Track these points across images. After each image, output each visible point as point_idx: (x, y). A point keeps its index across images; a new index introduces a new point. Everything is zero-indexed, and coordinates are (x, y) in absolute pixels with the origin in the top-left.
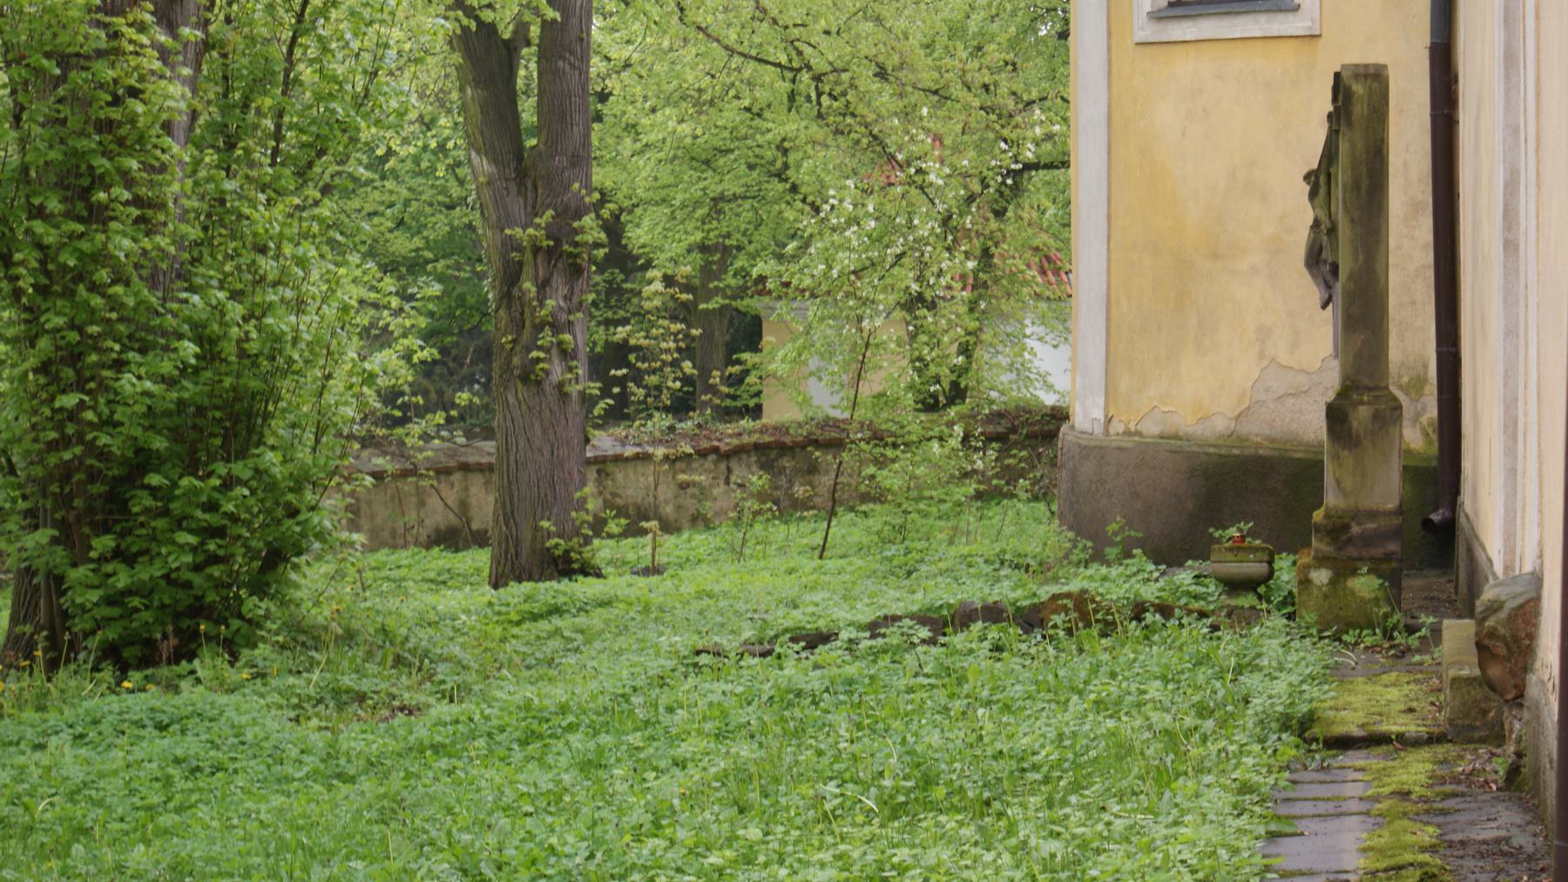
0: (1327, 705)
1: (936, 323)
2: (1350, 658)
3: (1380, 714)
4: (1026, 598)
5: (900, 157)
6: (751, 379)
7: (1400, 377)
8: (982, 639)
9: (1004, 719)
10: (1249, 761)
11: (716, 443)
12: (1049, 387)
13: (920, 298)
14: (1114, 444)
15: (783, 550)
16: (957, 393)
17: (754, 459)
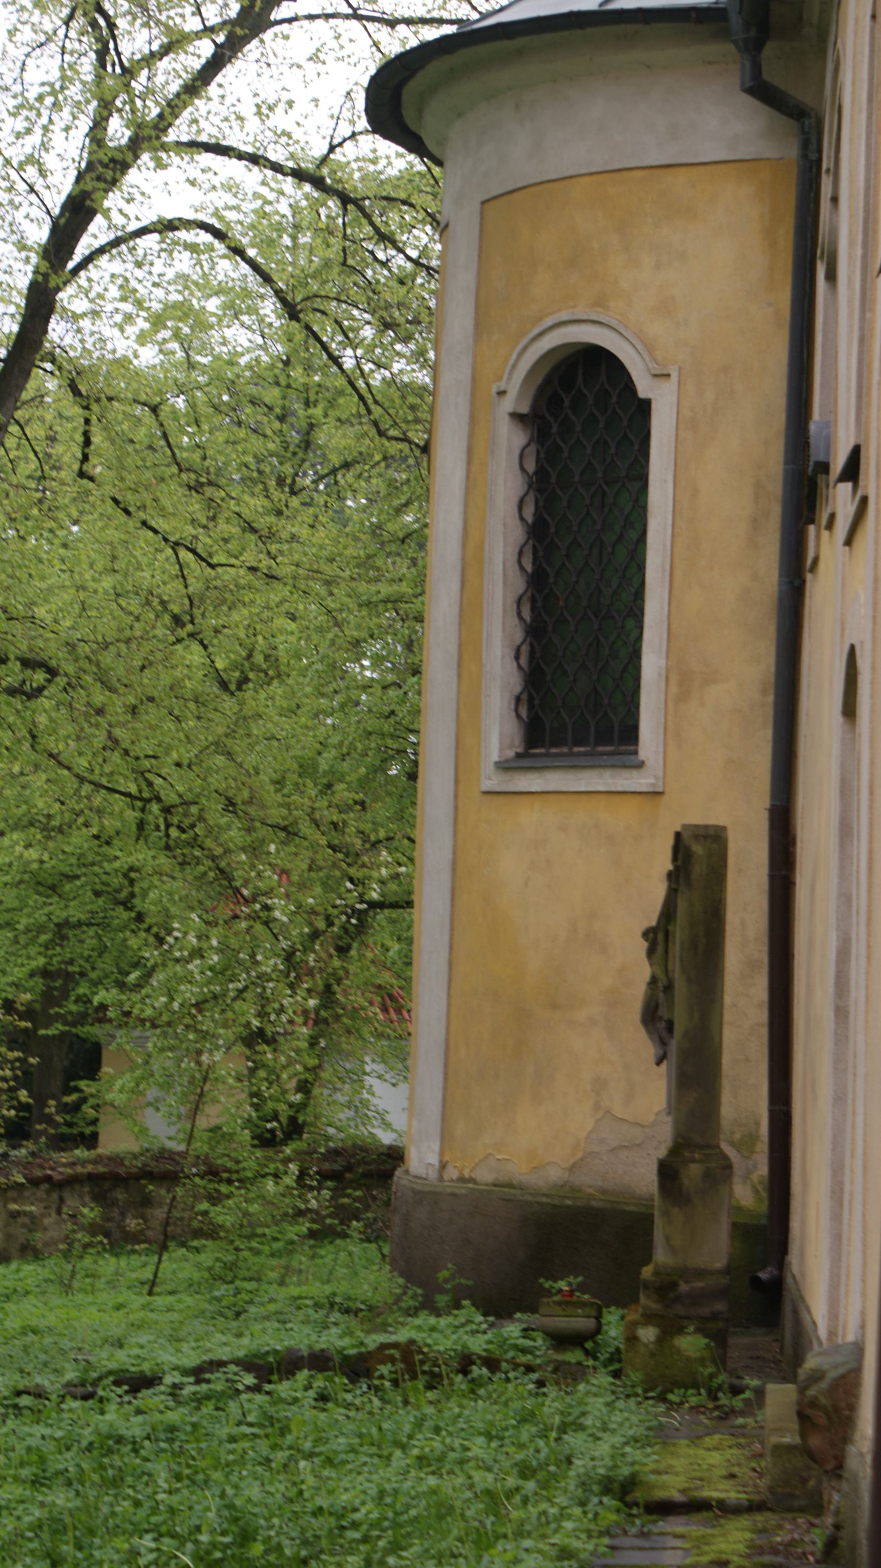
0: (647, 1469)
1: (275, 1060)
2: (675, 1419)
3: (701, 1479)
4: (353, 1346)
5: (245, 892)
6: (88, 1111)
7: (733, 1133)
8: (307, 1388)
9: (326, 1473)
10: (569, 1525)
11: (49, 1172)
12: (387, 1125)
13: (261, 1032)
14: (448, 1190)
15: (112, 1284)
16: (294, 1129)
17: (86, 1189)
